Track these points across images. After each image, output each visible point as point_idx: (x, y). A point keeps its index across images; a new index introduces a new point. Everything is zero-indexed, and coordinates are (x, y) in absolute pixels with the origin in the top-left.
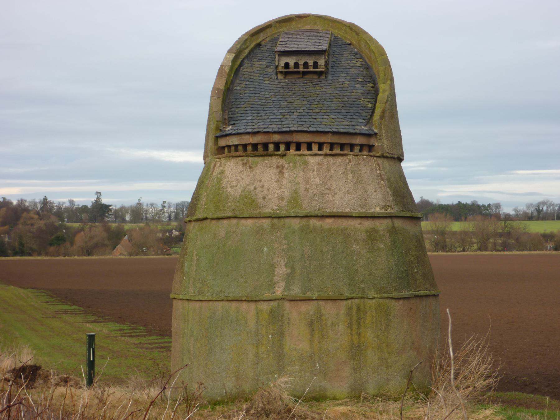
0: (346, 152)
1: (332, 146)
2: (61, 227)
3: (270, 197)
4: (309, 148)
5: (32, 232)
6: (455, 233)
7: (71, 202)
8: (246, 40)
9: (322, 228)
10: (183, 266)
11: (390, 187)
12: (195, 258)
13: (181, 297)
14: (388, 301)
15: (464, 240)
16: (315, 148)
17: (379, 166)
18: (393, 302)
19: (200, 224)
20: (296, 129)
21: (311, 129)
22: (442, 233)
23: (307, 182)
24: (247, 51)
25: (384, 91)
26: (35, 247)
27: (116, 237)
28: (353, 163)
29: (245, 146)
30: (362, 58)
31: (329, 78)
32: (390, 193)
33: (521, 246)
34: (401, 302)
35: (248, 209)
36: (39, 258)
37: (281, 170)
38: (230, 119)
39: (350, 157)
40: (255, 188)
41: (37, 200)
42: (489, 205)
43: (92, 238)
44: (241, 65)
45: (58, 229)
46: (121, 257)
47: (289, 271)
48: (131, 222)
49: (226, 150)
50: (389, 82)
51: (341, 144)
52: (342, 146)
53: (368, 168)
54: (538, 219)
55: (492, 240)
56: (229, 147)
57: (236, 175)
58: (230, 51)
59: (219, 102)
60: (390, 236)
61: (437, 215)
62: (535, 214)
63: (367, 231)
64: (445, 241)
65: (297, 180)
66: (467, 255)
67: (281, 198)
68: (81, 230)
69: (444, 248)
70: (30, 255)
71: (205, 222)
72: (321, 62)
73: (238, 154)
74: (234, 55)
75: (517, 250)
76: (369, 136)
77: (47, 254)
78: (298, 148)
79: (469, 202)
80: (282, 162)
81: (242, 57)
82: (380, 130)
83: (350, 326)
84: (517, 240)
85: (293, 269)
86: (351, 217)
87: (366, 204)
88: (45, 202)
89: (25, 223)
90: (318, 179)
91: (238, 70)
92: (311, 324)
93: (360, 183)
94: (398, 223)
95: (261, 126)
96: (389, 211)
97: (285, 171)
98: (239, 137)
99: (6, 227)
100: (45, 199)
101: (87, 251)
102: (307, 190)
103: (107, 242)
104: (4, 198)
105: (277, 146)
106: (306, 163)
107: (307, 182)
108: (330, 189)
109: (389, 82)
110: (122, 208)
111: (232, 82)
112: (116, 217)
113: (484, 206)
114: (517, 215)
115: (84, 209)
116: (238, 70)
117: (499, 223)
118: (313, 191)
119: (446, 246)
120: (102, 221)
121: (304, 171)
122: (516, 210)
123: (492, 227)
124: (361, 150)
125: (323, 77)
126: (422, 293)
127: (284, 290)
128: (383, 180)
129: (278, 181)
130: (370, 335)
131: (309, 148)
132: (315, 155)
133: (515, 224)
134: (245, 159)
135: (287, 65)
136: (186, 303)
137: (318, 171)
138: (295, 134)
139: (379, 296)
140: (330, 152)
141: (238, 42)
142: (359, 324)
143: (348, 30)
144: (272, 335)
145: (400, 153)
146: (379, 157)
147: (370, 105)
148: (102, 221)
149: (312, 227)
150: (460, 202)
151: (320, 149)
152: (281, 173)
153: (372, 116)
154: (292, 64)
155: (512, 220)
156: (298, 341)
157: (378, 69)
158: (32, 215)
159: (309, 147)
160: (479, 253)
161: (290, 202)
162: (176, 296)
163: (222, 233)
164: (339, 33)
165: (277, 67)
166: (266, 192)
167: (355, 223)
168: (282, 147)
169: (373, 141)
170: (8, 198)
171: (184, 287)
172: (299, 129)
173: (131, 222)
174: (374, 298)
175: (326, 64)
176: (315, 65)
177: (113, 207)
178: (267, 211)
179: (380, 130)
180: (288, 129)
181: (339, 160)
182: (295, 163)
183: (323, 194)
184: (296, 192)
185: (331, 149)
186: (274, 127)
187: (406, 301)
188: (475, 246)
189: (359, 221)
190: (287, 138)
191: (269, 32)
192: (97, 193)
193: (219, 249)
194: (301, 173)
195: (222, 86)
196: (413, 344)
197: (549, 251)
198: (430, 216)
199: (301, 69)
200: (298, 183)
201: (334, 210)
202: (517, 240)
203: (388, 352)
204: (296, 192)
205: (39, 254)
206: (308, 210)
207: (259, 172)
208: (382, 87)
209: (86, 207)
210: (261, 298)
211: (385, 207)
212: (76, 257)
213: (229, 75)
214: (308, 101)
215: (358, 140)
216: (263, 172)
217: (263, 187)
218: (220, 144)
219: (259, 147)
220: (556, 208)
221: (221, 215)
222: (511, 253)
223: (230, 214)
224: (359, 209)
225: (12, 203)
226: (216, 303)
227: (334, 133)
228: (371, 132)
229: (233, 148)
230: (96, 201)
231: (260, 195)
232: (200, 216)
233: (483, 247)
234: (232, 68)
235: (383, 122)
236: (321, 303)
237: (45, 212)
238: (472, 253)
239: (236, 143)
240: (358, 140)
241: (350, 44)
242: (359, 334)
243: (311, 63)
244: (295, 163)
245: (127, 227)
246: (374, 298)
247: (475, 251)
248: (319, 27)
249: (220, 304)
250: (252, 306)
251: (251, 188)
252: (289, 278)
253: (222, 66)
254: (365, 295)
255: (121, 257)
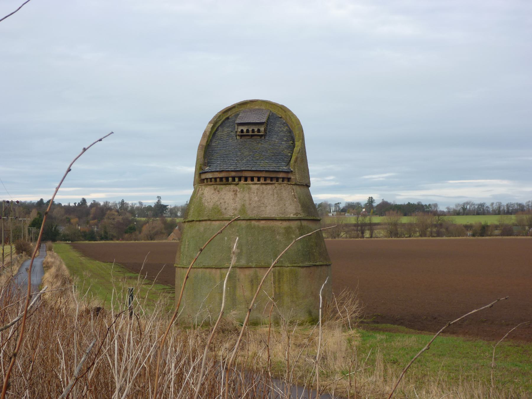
0: (273, 182)
1: (265, 179)
2: (133, 221)
3: (229, 208)
4: (252, 179)
5: (112, 224)
6: (404, 225)
7: (141, 203)
8: (220, 116)
9: (258, 226)
10: (180, 248)
11: (300, 202)
12: (187, 243)
13: (179, 266)
14: (296, 268)
15: (410, 229)
16: (256, 180)
17: (293, 190)
18: (300, 269)
19: (190, 224)
20: (244, 169)
21: (253, 169)
22: (395, 225)
23: (250, 200)
24: (220, 122)
25: (298, 146)
26: (115, 234)
27: (170, 227)
28: (277, 188)
29: (216, 179)
30: (287, 126)
31: (267, 138)
32: (300, 205)
33: (449, 233)
34: (305, 269)
35: (216, 215)
36: (118, 242)
37: (235, 192)
38: (208, 163)
39: (276, 185)
40: (221, 203)
41: (117, 202)
42: (430, 205)
43: (154, 228)
44: (217, 130)
45: (131, 222)
46: (174, 241)
47: (239, 251)
48: (181, 217)
49: (205, 181)
50: (301, 141)
51: (271, 178)
52: (272, 179)
53: (286, 192)
54: (463, 214)
55: (429, 230)
56: (207, 179)
57: (211, 195)
58: (210, 123)
59: (202, 153)
60: (299, 231)
61: (391, 212)
62: (461, 211)
63: (285, 228)
64: (397, 230)
65: (244, 198)
66: (412, 240)
67: (235, 209)
68: (145, 223)
69: (396, 235)
70: (112, 240)
71: (192, 223)
72: (262, 129)
73: (211, 183)
74: (212, 125)
75: (446, 236)
76: (287, 172)
77: (123, 239)
78: (246, 180)
79: (416, 203)
80: (236, 188)
81: (217, 126)
82: (294, 169)
83: (274, 283)
84: (447, 229)
85: (241, 250)
86: (276, 220)
87: (285, 213)
88: (123, 203)
89: (109, 218)
90: (256, 198)
91: (215, 133)
92: (252, 281)
93: (281, 200)
94: (304, 223)
95: (224, 167)
96: (299, 216)
97: (238, 193)
98: (212, 174)
99: (96, 221)
100: (123, 201)
101: (151, 237)
102: (250, 204)
103: (164, 231)
104: (94, 201)
105: (234, 179)
106: (250, 189)
107: (250, 200)
108: (264, 204)
109: (301, 141)
110: (175, 207)
111: (211, 141)
112: (171, 214)
113: (426, 205)
114: (449, 212)
115: (149, 208)
116: (215, 133)
117: (434, 217)
118: (254, 204)
119: (397, 234)
120: (162, 216)
121: (248, 193)
122: (448, 208)
123: (430, 220)
124: (283, 181)
125: (263, 138)
126: (318, 263)
127: (237, 262)
128: (295, 198)
129: (233, 199)
130: (286, 288)
131: (252, 179)
132: (256, 184)
133: (446, 218)
134: (216, 186)
135: (242, 131)
136: (182, 269)
137: (257, 193)
138: (243, 172)
139: (291, 265)
140: (264, 182)
141: (215, 117)
142: (279, 281)
143: (280, 110)
144: (229, 287)
145: (307, 182)
146: (294, 185)
147: (290, 154)
148: (162, 216)
149: (253, 226)
150: (409, 203)
151: (259, 180)
152: (236, 194)
153: (290, 161)
154: (245, 130)
155: (445, 215)
156: (244, 291)
157: (296, 133)
158: (113, 212)
159: (252, 179)
160: (420, 238)
161: (240, 211)
162: (177, 265)
163: (202, 229)
164: (275, 111)
165: (236, 132)
166: (227, 205)
167: (278, 223)
168: (237, 180)
169: (290, 176)
170: (97, 201)
171: (181, 260)
172: (246, 169)
173: (181, 217)
174: (288, 267)
175: (265, 130)
176: (259, 131)
177: (169, 207)
178: (227, 216)
179: (294, 169)
180: (240, 169)
181: (269, 187)
182: (244, 188)
183: (259, 207)
184: (244, 205)
185: (265, 180)
186: (232, 168)
187: (308, 268)
188: (418, 234)
189: (280, 222)
190: (239, 174)
191: (234, 111)
192: (158, 197)
193: (200, 238)
194: (247, 195)
195: (204, 144)
196: (312, 293)
197: (468, 237)
198: (387, 213)
199: (250, 133)
200: (245, 200)
201: (266, 216)
202: (447, 229)
203: (297, 298)
204: (244, 205)
205: (118, 239)
206: (251, 216)
207: (223, 194)
208: (297, 143)
209: (150, 206)
210: (223, 266)
211: (296, 214)
212: (143, 241)
213: (209, 136)
214: (253, 152)
215: (281, 175)
216: (225, 194)
217: (225, 202)
218: (202, 179)
219: (224, 179)
220: (476, 207)
221: (201, 219)
222: (442, 238)
223: (206, 218)
224: (281, 215)
225: (100, 204)
226: (198, 269)
227: (266, 171)
228: (289, 170)
229: (209, 180)
230: (158, 202)
231: (223, 207)
232: (190, 219)
233: (423, 234)
234: (211, 132)
235: (296, 164)
236: (257, 269)
237: (123, 211)
238: (415, 238)
239: (211, 177)
240: (281, 175)
241: (281, 118)
242: (279, 287)
243: (256, 130)
244: (244, 188)
245: (178, 220)
246: (288, 267)
247: (418, 237)
248: (263, 107)
249: (200, 270)
250: (218, 271)
251: (219, 203)
252: (239, 255)
253: (205, 131)
254: (283, 265)
255: (174, 241)
